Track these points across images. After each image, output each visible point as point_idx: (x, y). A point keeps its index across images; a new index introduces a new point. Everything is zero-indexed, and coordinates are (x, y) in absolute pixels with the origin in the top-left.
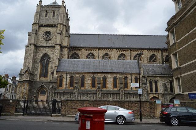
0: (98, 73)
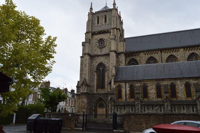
0: (164, 80)
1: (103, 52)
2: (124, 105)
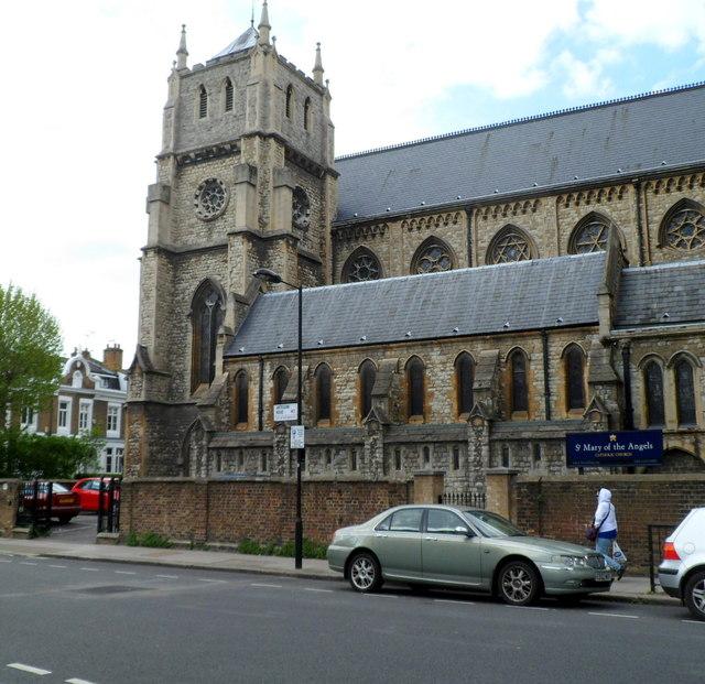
0: (386, 346)
1: (215, 236)
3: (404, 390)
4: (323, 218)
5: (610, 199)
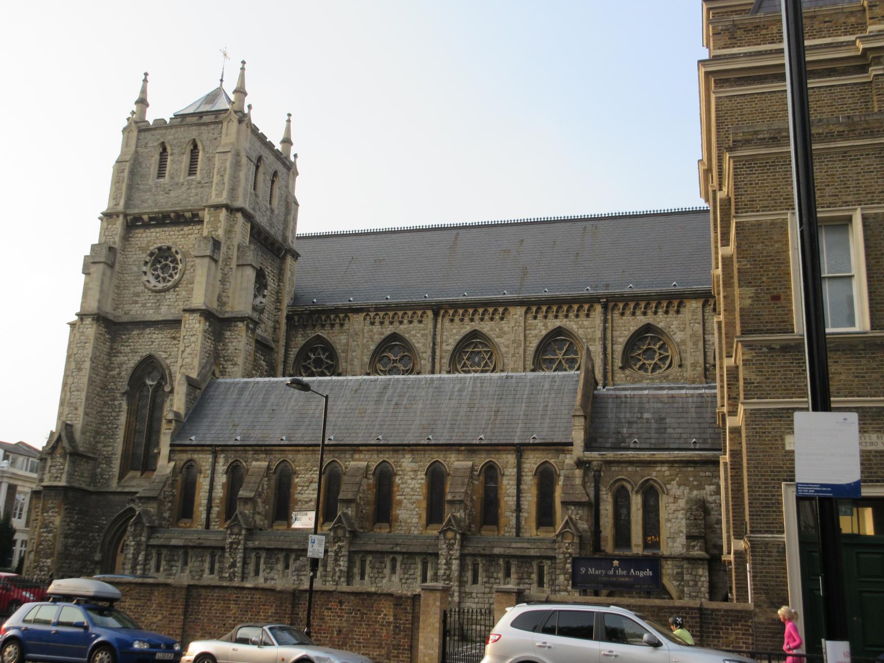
0: (355, 448)
1: (164, 309)
2: (185, 548)
3: (371, 496)
4: (279, 301)
5: (577, 316)
